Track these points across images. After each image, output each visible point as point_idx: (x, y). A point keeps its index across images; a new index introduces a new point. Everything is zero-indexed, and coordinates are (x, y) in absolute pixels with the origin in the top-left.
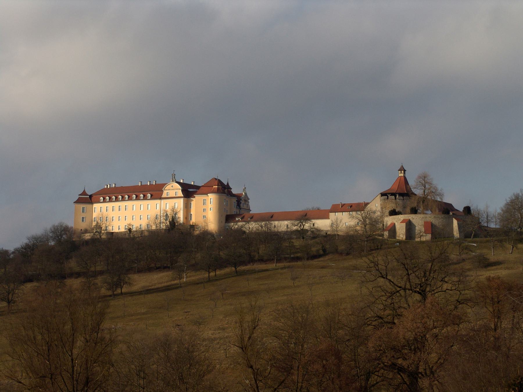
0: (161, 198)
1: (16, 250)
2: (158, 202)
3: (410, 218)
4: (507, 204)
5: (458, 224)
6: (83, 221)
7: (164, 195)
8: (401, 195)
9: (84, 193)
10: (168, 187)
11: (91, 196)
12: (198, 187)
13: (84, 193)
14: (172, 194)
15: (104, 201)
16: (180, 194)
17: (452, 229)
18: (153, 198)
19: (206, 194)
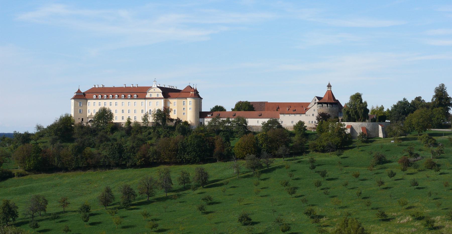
0: (145, 99)
1: (49, 128)
2: (139, 102)
3: (352, 124)
4: (395, 106)
5: (382, 128)
6: (80, 112)
7: (148, 96)
8: (331, 104)
9: (79, 91)
10: (151, 90)
11: (84, 94)
12: (179, 91)
13: (79, 91)
14: (154, 95)
15: (97, 98)
16: (161, 95)
17: (436, 128)
18: (138, 98)
19: (186, 98)
